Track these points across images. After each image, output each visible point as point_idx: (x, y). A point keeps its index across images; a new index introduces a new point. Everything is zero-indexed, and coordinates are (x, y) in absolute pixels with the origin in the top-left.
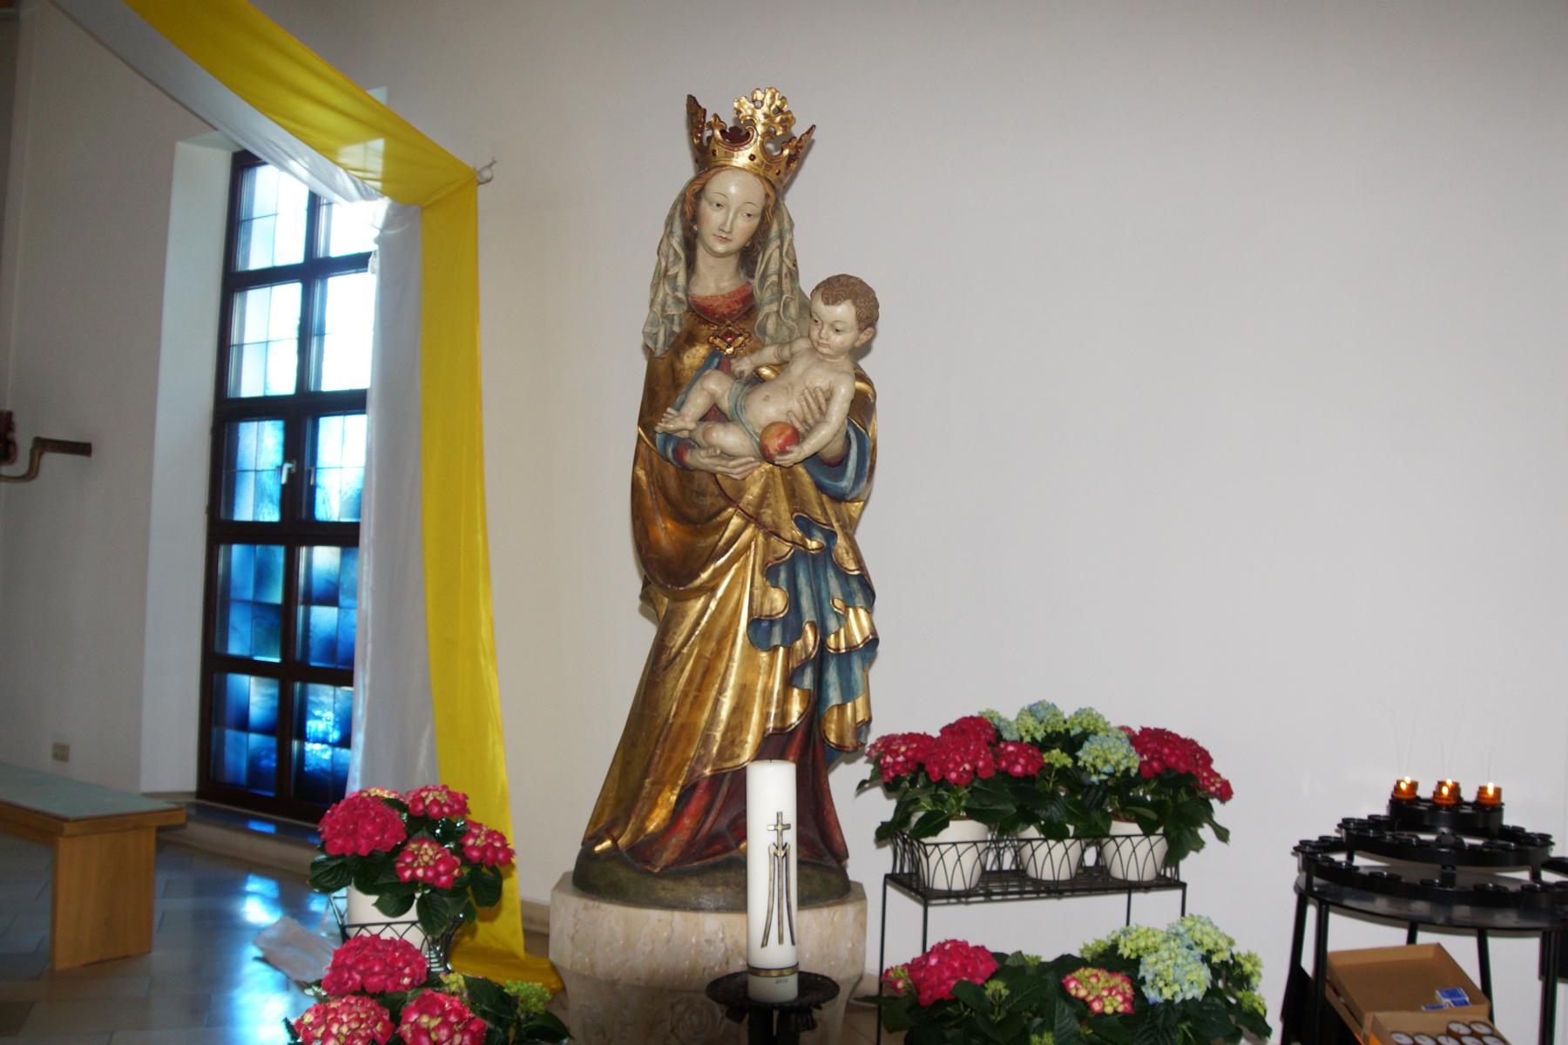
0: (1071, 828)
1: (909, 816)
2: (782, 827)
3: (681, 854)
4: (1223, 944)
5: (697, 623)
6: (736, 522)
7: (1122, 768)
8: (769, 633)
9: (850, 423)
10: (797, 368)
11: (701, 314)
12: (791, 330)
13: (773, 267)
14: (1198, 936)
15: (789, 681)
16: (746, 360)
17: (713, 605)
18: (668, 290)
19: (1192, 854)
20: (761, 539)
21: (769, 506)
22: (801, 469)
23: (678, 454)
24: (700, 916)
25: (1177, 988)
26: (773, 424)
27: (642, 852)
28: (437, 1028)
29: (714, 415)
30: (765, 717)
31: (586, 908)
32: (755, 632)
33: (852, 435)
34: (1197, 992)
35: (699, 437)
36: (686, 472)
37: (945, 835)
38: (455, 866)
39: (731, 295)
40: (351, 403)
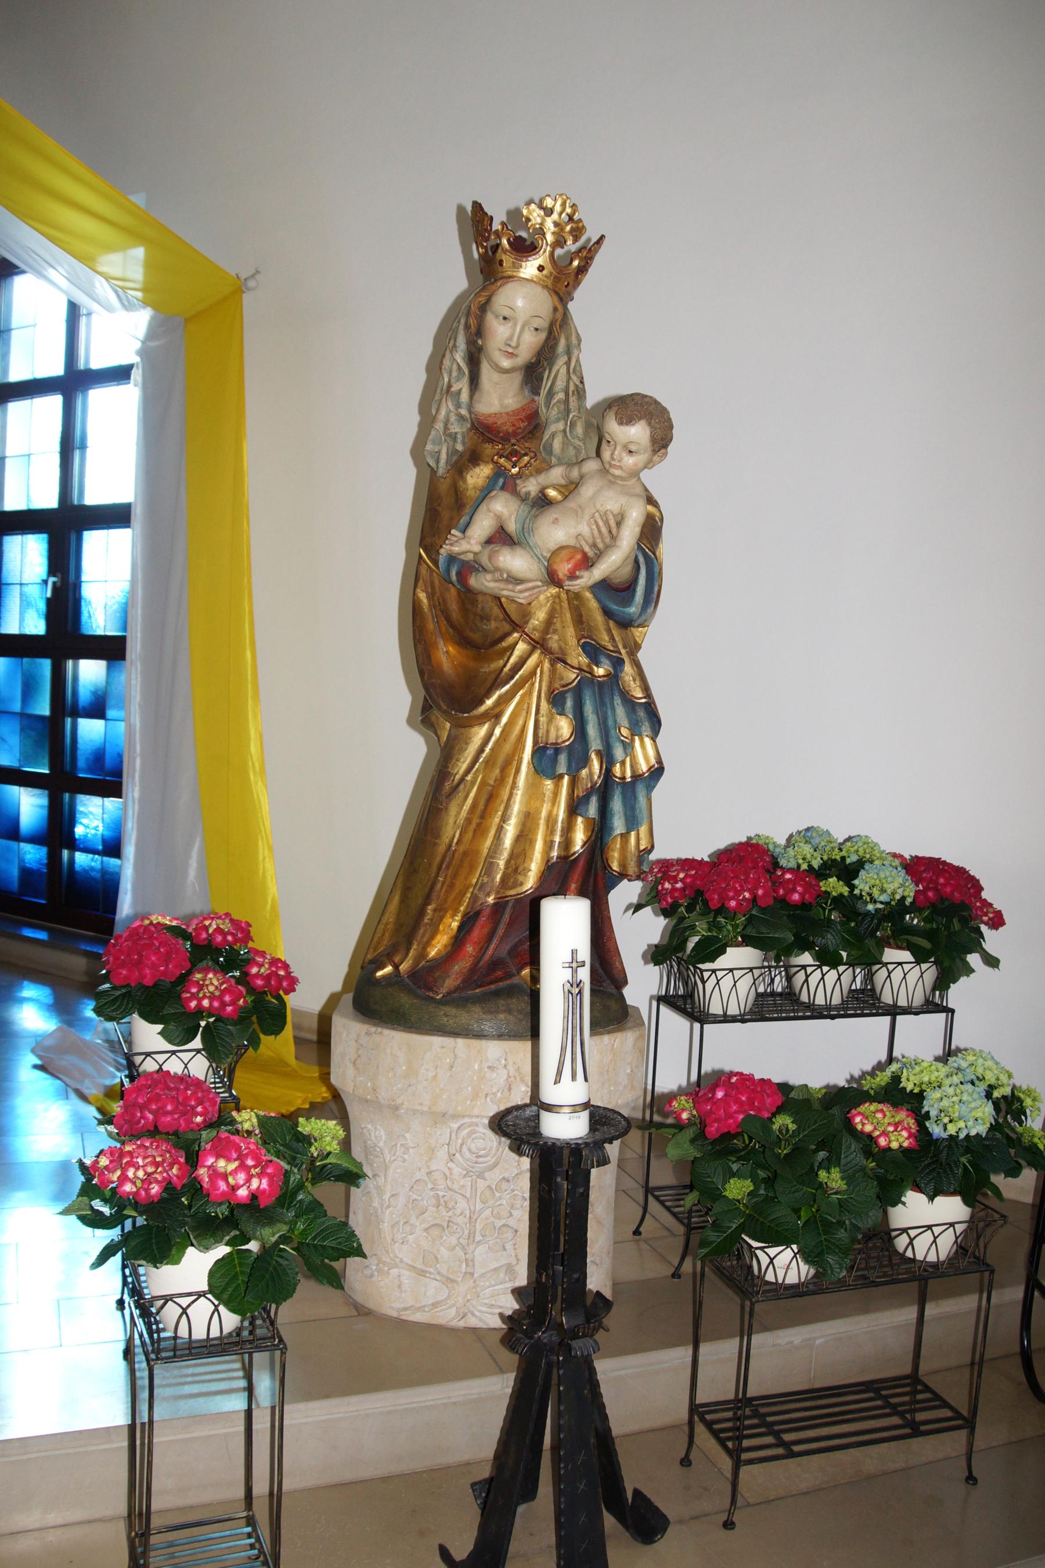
0: (844, 954)
1: (685, 941)
2: (574, 964)
3: (463, 982)
4: (1004, 1078)
5: (481, 750)
6: (521, 647)
7: (898, 897)
8: (554, 760)
9: (639, 547)
10: (587, 491)
11: (485, 431)
12: (577, 449)
13: (560, 384)
14: (980, 1071)
15: (574, 809)
16: (533, 480)
17: (498, 731)
18: (451, 407)
19: (963, 980)
20: (547, 665)
21: (555, 631)
22: (588, 595)
23: (462, 576)
24: (484, 1043)
25: (962, 1124)
26: (562, 548)
27: (424, 978)
28: (234, 1172)
29: (501, 537)
30: (549, 845)
31: (368, 1034)
32: (540, 760)
33: (641, 559)
34: (982, 1129)
35: (484, 560)
36: (468, 596)
37: (722, 962)
38: (240, 995)
39: (515, 412)
40: (115, 516)
